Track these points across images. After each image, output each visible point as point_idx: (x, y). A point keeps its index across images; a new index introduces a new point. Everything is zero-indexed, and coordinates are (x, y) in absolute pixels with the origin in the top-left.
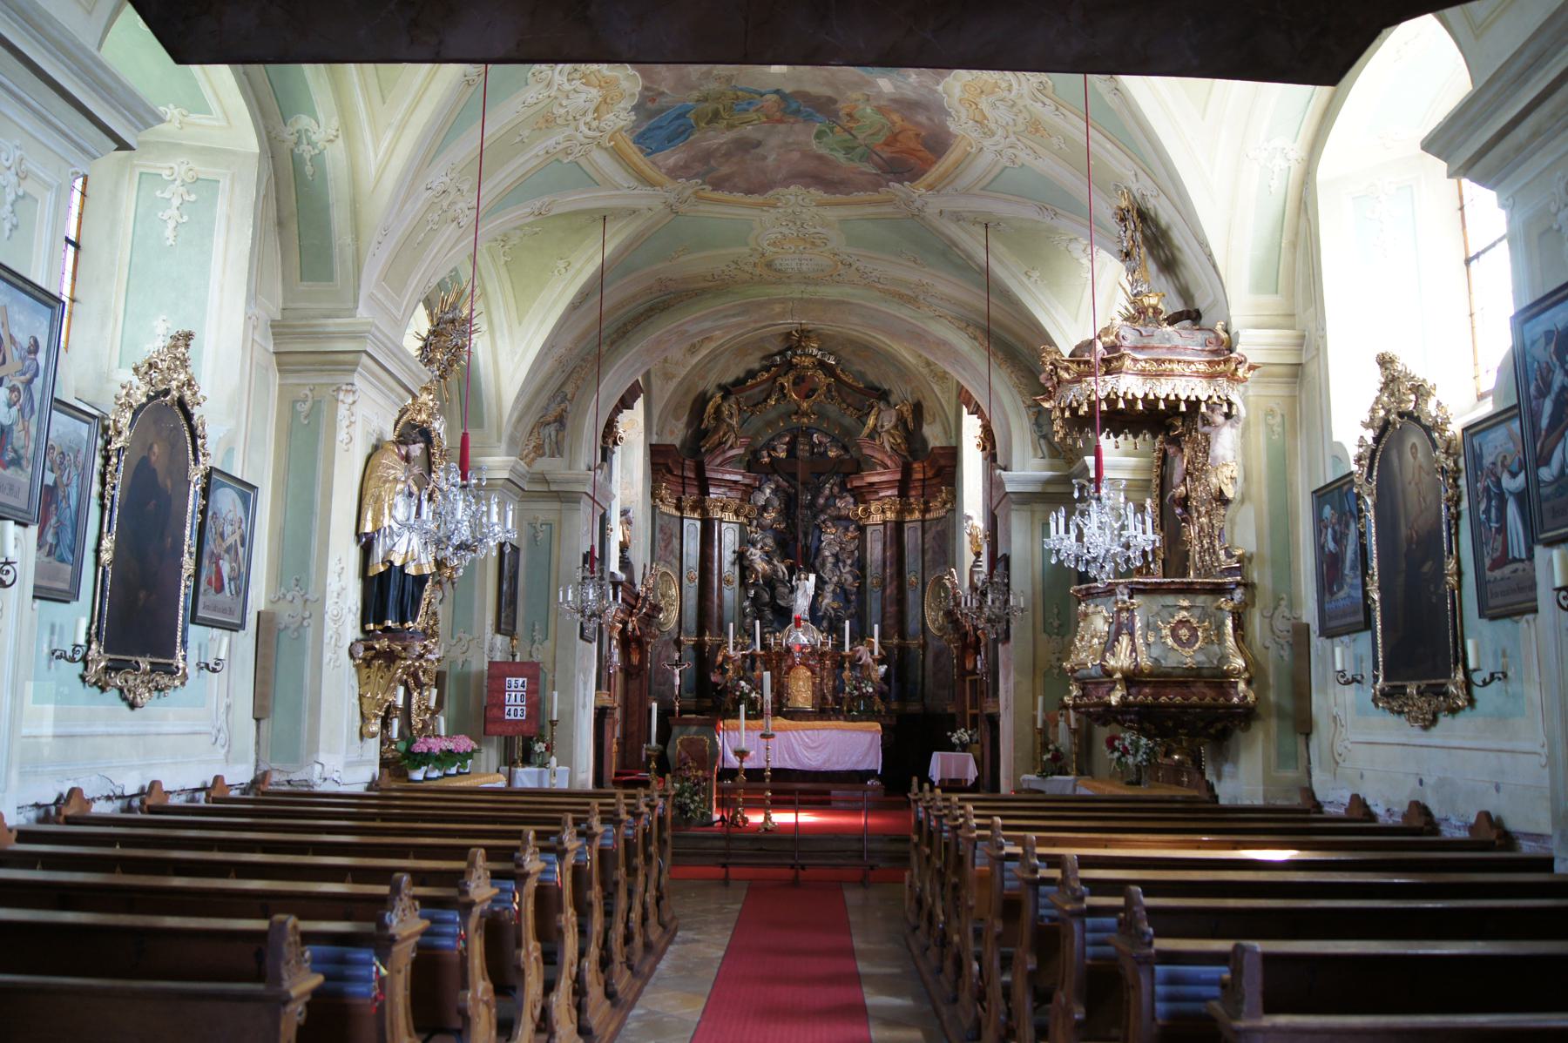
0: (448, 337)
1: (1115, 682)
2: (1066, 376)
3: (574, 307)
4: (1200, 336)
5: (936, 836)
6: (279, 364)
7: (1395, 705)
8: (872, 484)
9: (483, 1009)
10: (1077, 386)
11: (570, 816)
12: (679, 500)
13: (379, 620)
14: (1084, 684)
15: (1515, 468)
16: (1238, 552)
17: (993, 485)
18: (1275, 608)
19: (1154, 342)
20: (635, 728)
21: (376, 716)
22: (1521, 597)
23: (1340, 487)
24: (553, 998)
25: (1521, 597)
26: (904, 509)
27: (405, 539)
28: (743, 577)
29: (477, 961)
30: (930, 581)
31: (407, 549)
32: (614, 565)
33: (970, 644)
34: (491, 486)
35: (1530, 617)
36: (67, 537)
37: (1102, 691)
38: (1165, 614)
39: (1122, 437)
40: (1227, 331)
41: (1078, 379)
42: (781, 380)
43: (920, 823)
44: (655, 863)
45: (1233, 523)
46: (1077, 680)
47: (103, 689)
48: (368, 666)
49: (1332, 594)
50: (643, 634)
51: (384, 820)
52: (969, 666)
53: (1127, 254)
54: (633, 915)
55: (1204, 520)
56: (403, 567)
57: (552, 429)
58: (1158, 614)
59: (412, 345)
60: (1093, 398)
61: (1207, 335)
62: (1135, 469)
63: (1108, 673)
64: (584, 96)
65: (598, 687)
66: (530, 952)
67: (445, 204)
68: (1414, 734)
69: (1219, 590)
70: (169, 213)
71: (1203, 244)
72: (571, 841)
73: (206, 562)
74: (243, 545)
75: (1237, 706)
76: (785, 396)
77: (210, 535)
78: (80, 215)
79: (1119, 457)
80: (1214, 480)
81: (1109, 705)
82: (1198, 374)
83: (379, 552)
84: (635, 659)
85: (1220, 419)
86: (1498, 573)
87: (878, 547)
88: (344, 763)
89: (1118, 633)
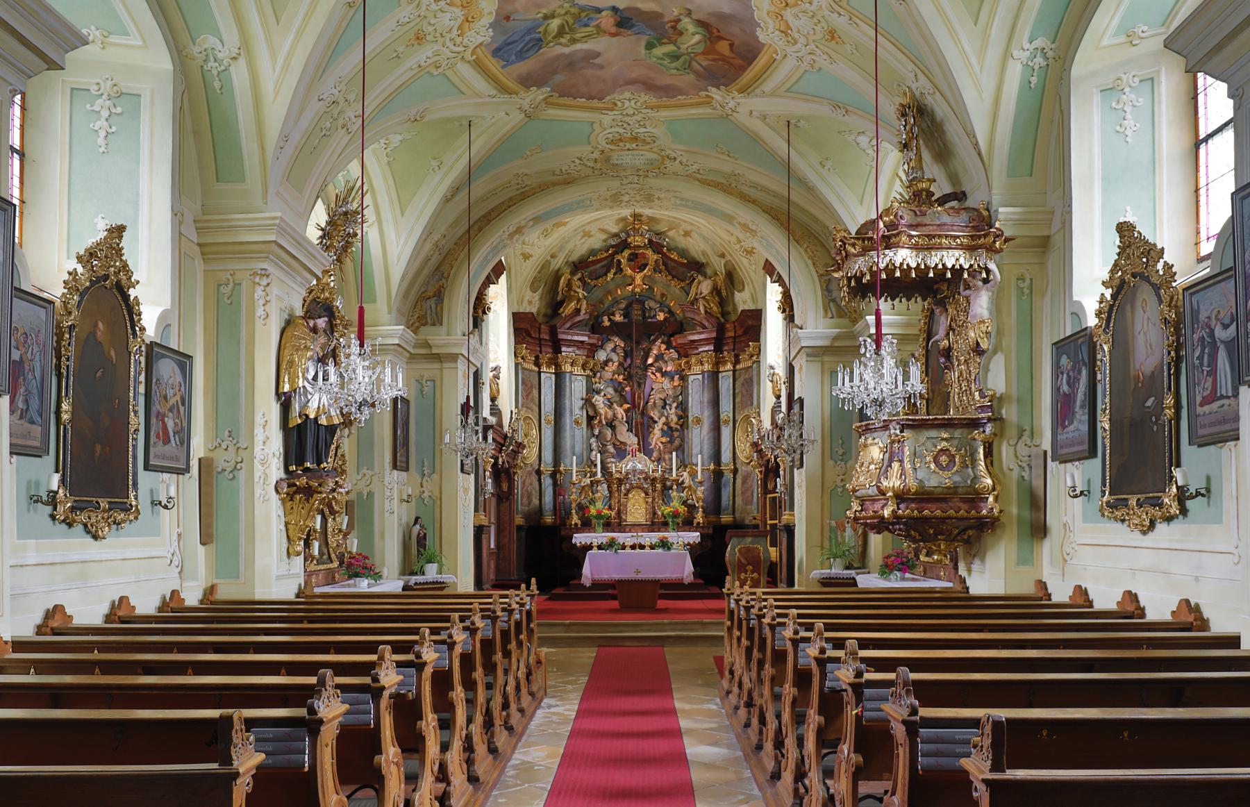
0: (342, 229)
3: (447, 200)
4: (964, 216)
5: (744, 623)
6: (203, 254)
7: (1118, 513)
9: (393, 768)
11: (457, 615)
12: (537, 358)
13: (300, 462)
14: (863, 501)
15: (1227, 321)
16: (991, 393)
19: (926, 220)
20: (506, 540)
21: (300, 539)
22: (1227, 427)
24: (448, 755)
25: (1227, 427)
26: (718, 363)
27: (316, 397)
28: (590, 419)
29: (387, 732)
30: (739, 418)
31: (318, 403)
32: (486, 412)
34: (384, 349)
35: (1232, 443)
36: (35, 403)
37: (877, 506)
38: (929, 444)
42: (618, 257)
43: (732, 612)
44: (525, 648)
45: (987, 370)
46: (857, 498)
47: (70, 525)
48: (292, 500)
49: (1064, 427)
50: (510, 467)
51: (310, 622)
52: (770, 487)
53: (905, 146)
54: (508, 688)
56: (316, 419)
57: (432, 302)
59: (313, 234)
60: (875, 268)
63: (882, 493)
64: (448, 15)
65: (476, 510)
66: (429, 723)
67: (335, 113)
68: (1136, 538)
69: (974, 424)
70: (99, 123)
72: (459, 636)
73: (153, 420)
74: (183, 404)
76: (621, 270)
77: (155, 398)
78: (22, 126)
79: (893, 316)
81: (883, 517)
83: (296, 407)
84: (505, 487)
86: (1207, 408)
88: (276, 575)
89: (891, 461)
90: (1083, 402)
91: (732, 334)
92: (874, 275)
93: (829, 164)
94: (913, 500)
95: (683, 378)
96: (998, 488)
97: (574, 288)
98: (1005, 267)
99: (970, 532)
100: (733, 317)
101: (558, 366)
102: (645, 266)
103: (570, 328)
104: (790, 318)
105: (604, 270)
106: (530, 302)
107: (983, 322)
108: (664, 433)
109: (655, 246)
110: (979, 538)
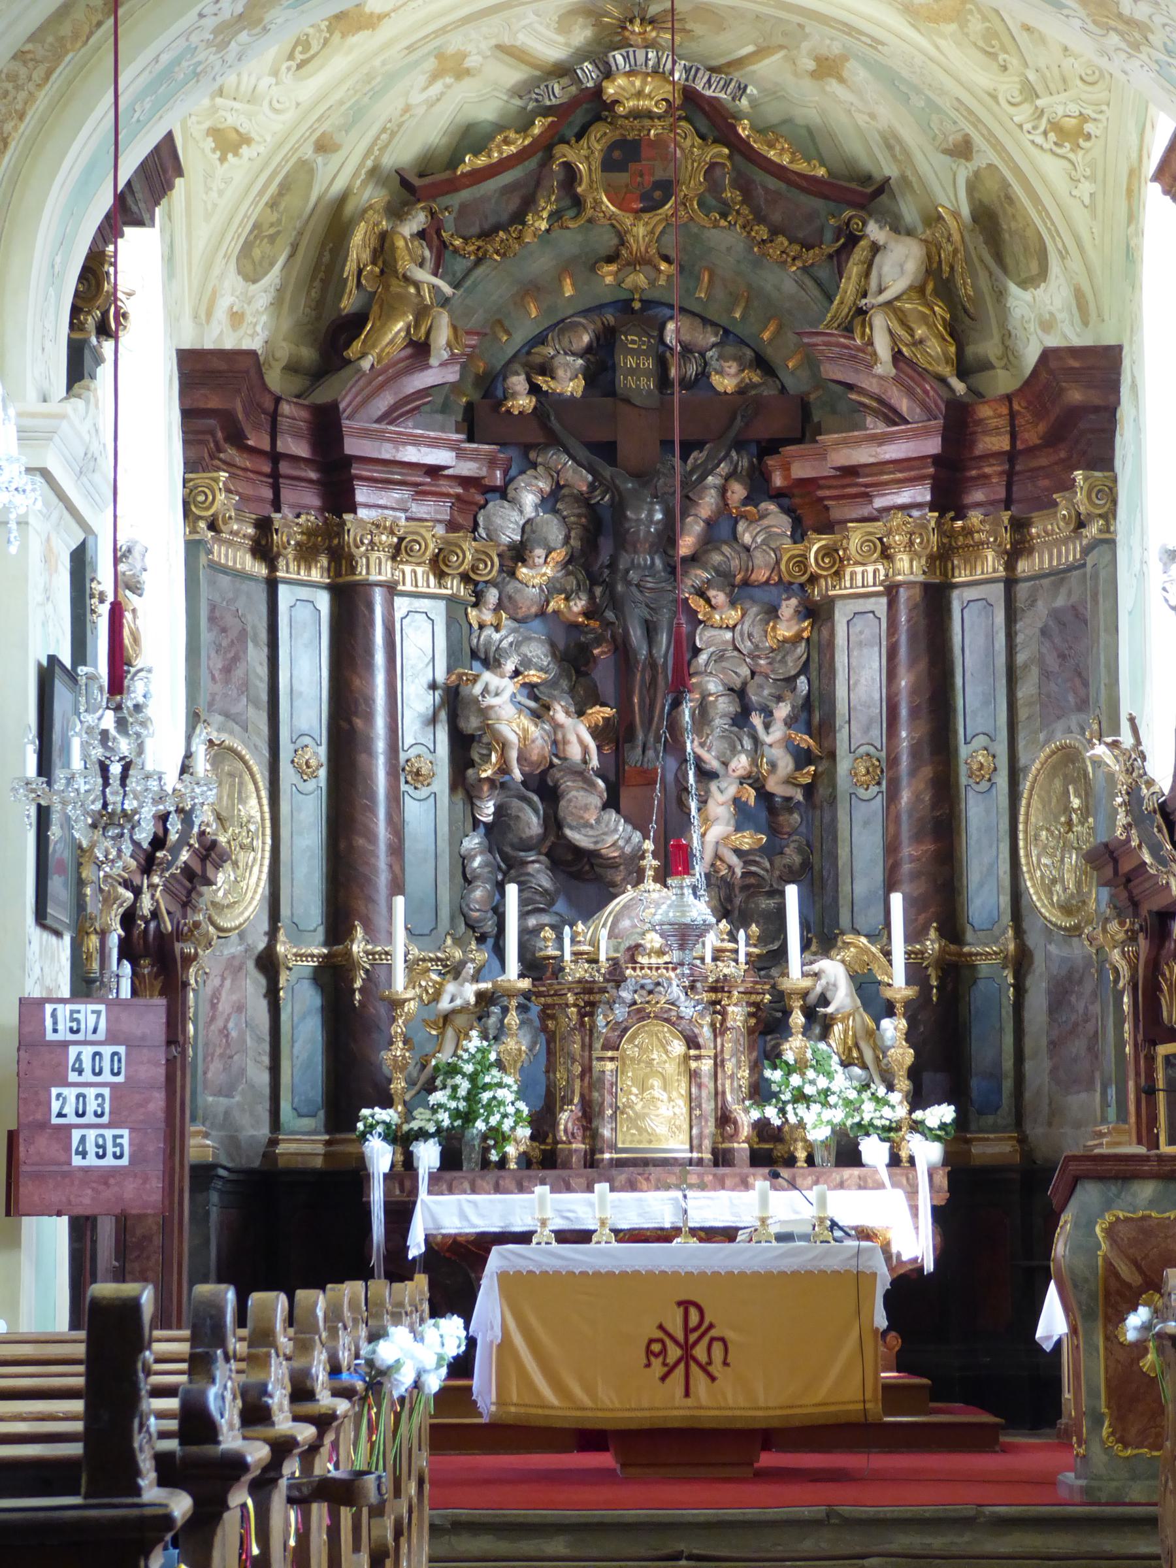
8: (851, 471)
12: (264, 526)
30: (1035, 762)
76: (577, 203)
95: (817, 613)
97: (406, 265)
100: (1003, 382)
101: (341, 559)
102: (666, 188)
103: (389, 417)
105: (514, 204)
106: (236, 318)
108: (742, 816)
109: (703, 114)
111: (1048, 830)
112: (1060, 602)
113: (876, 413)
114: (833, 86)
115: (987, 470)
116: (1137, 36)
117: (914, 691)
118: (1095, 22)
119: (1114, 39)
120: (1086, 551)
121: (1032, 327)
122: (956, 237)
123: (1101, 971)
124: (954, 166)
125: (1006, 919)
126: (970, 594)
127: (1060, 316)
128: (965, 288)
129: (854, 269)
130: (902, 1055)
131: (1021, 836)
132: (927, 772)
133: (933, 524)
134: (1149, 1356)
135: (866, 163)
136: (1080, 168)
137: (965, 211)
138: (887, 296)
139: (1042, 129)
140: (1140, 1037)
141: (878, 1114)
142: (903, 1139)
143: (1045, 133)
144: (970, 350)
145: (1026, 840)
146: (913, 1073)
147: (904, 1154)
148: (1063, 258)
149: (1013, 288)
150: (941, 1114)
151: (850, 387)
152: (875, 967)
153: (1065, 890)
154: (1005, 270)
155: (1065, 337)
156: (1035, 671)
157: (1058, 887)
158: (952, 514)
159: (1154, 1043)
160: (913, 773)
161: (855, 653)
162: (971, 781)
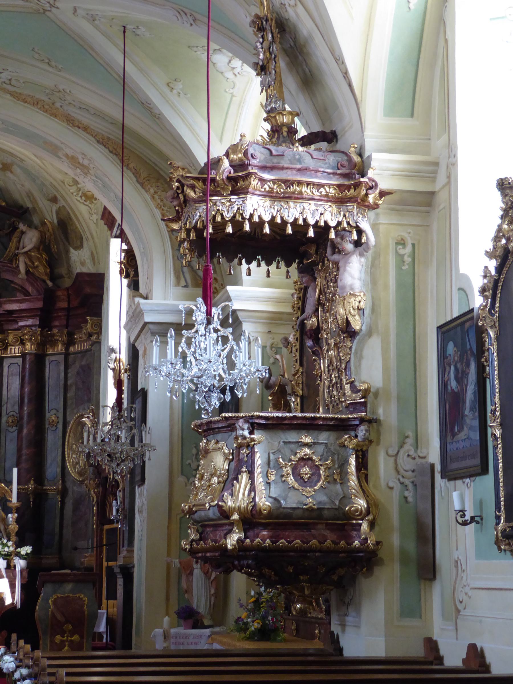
1: (232, 524)
2: (192, 194)
4: (332, 159)
8: (11, 312)
10: (203, 207)
16: (363, 387)
17: (135, 314)
18: (401, 447)
23: (463, 324)
33: (107, 488)
37: (219, 533)
38: (287, 450)
39: (254, 264)
40: (360, 155)
41: (203, 199)
49: (454, 435)
55: (332, 353)
58: (279, 451)
61: (341, 158)
62: (278, 301)
63: (225, 514)
69: (342, 426)
71: (340, 61)
75: (358, 550)
80: (341, 311)
82: (327, 198)
85: (350, 247)
87: (16, 383)
90: (472, 402)
91: (64, 305)
92: (220, 227)
93: (179, 86)
94: (265, 526)
96: (373, 510)
98: (382, 228)
99: (341, 571)
100: (68, 282)
104: (134, 286)
107: (354, 295)
110: (353, 580)
111: (75, 445)
112: (83, 363)
113: (20, 291)
114: (8, 174)
115: (60, 314)
116: (86, 171)
117: (30, 393)
118: (72, 164)
119: (79, 171)
120: (92, 345)
121: (78, 264)
122: (51, 230)
123: (89, 497)
124: (51, 205)
125: (59, 477)
126: (53, 358)
127: (87, 261)
128: (54, 249)
129: (15, 239)
130: (14, 527)
131: (66, 447)
132: (33, 422)
133: (39, 333)
134: (66, 648)
135: (21, 202)
136: (93, 210)
137: (55, 221)
138: (25, 250)
139: (80, 195)
140: (98, 523)
141: (3, 550)
142: (12, 559)
143: (81, 197)
144: (56, 271)
145: (68, 448)
146: (17, 534)
147: (12, 565)
148: (87, 241)
149: (72, 250)
150: (26, 550)
151: (12, 282)
152: (7, 495)
153: (80, 467)
154: (69, 243)
155: (89, 269)
156: (74, 388)
157: (78, 466)
158: (47, 329)
159: (103, 524)
160: (28, 423)
161: (10, 378)
162: (49, 426)
